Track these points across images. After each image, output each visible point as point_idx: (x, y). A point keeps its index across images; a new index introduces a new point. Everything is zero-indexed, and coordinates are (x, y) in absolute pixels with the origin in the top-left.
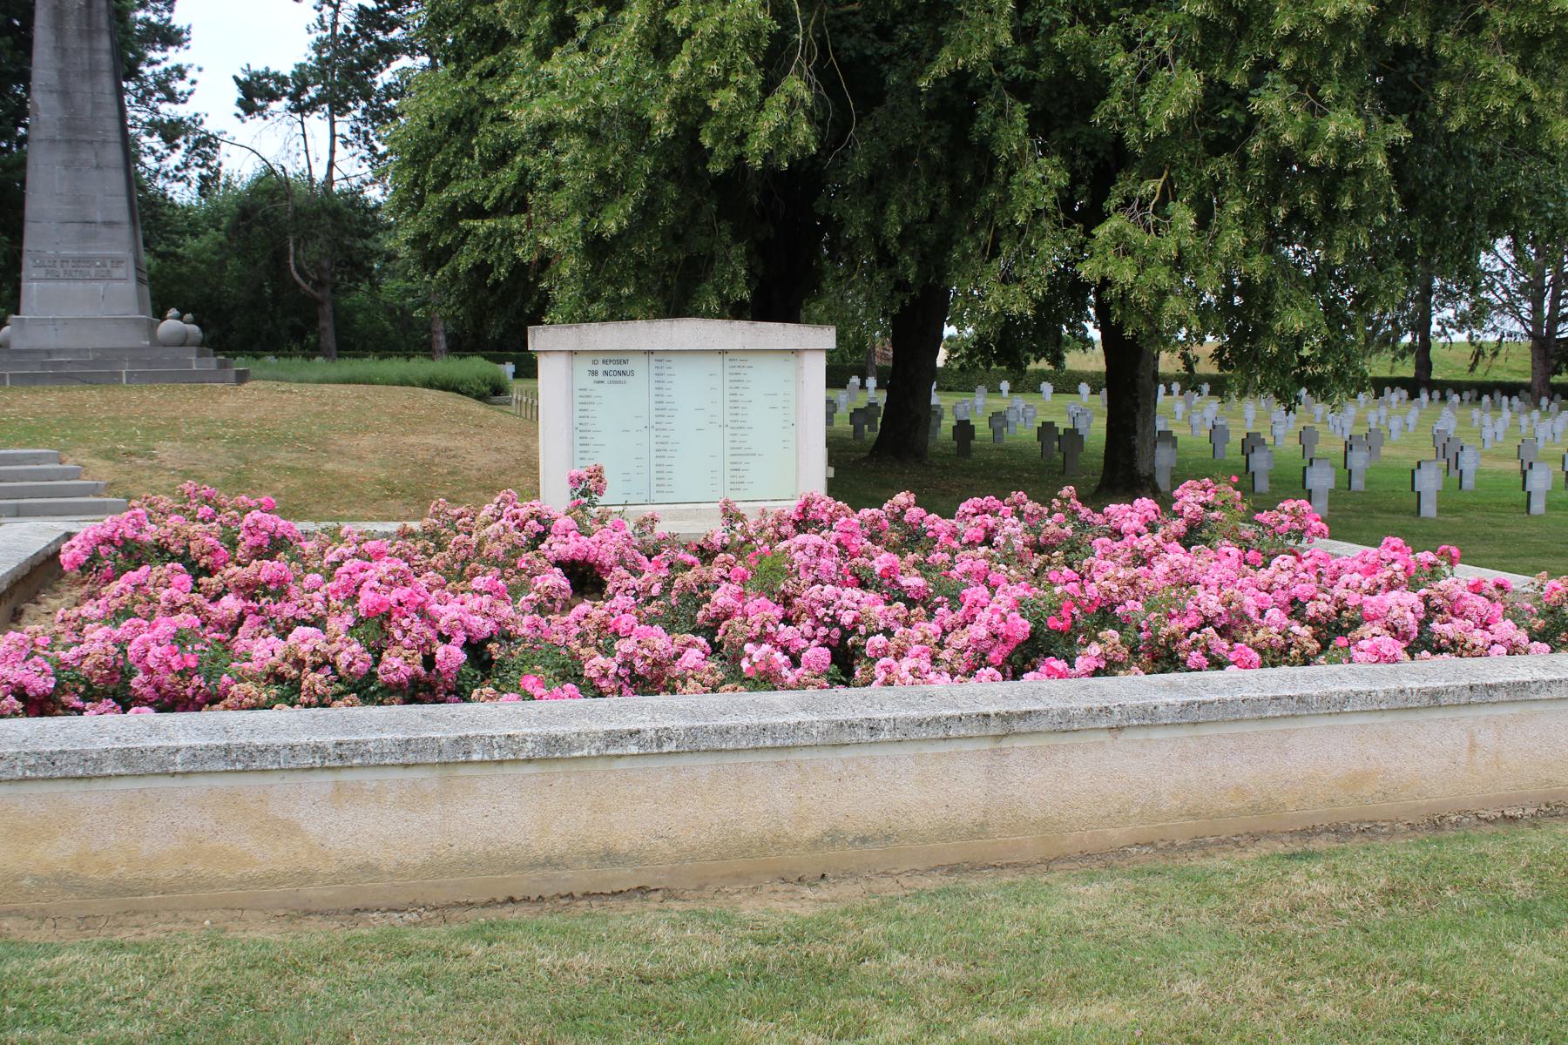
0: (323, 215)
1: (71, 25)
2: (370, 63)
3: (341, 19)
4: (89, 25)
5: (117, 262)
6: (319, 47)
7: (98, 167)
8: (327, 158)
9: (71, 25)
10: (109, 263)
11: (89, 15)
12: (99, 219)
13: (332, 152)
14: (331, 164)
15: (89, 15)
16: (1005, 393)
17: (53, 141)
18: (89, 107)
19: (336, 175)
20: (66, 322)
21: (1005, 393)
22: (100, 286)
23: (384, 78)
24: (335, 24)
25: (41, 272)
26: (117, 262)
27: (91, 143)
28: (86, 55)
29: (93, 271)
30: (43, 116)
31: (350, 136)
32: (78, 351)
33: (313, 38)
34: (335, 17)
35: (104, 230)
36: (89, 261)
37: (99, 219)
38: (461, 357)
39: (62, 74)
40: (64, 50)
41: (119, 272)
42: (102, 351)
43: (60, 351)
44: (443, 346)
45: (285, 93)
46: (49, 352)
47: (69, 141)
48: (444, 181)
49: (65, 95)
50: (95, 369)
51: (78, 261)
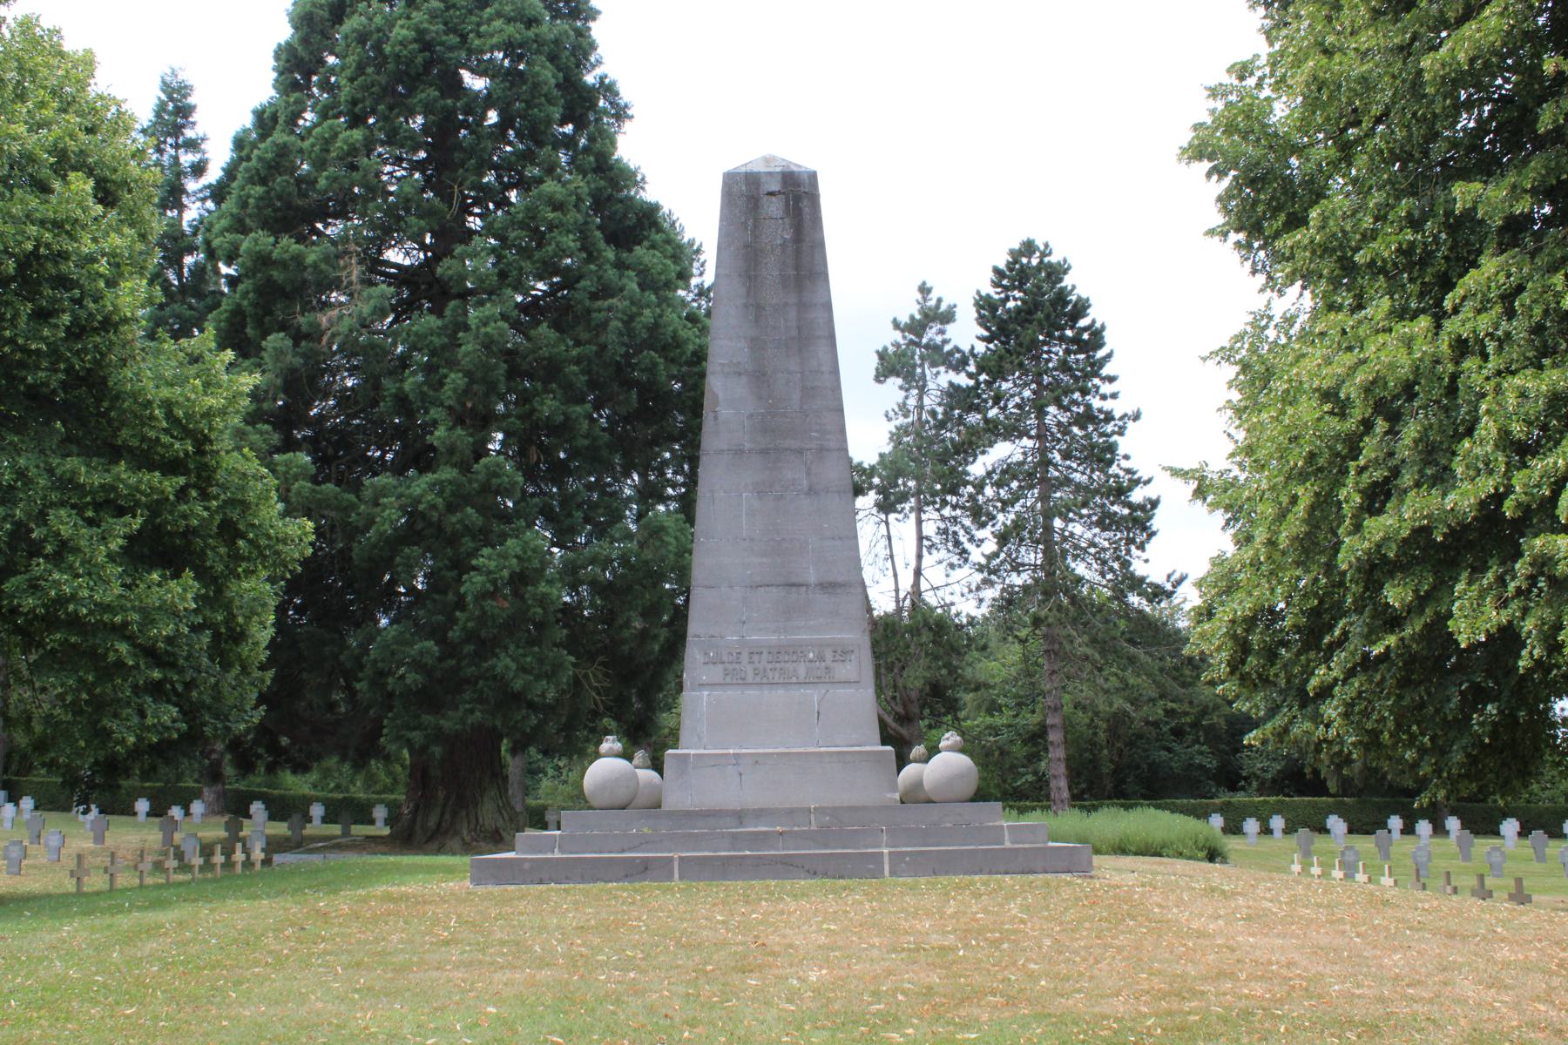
0: (925, 632)
1: (771, 269)
2: (970, 446)
3: (926, 401)
4: (797, 268)
5: (842, 653)
6: (896, 438)
7: (812, 491)
8: (913, 564)
9: (771, 269)
10: (829, 655)
11: (798, 253)
12: (812, 578)
13: (919, 557)
14: (918, 573)
15: (798, 253)
16: (141, 817)
17: (739, 452)
18: (796, 396)
19: (924, 585)
20: (757, 760)
21: (141, 817)
22: (814, 695)
23: (977, 469)
24: (920, 407)
25: (716, 673)
26: (842, 653)
27: (800, 452)
28: (793, 314)
29: (802, 669)
30: (725, 412)
31: (937, 539)
32: (791, 812)
33: (891, 426)
34: (921, 399)
35: (821, 598)
36: (794, 651)
37: (812, 578)
38: (1127, 807)
39: (756, 344)
40: (759, 308)
41: (846, 670)
42: (834, 811)
43: (760, 814)
44: (1066, 794)
45: (871, 487)
46: (740, 816)
47: (765, 452)
48: (1377, 497)
49: (760, 377)
50: (822, 850)
51: (778, 652)
